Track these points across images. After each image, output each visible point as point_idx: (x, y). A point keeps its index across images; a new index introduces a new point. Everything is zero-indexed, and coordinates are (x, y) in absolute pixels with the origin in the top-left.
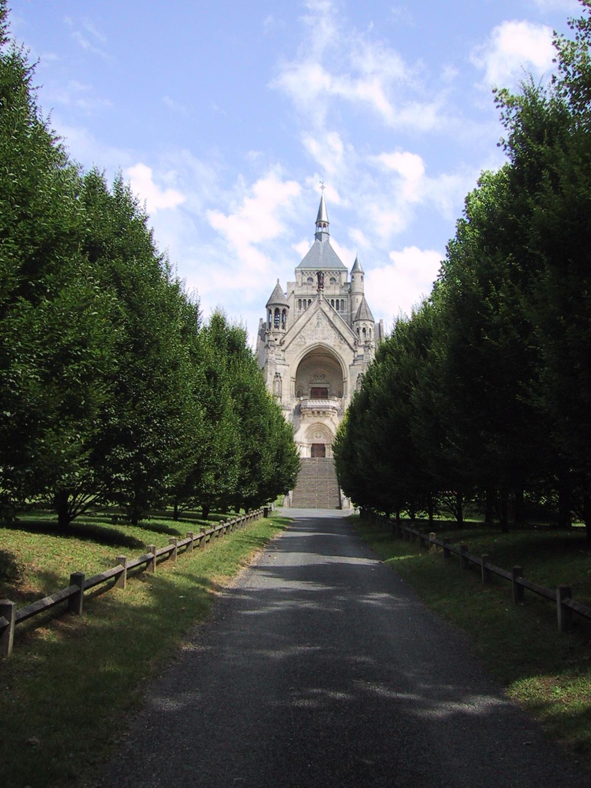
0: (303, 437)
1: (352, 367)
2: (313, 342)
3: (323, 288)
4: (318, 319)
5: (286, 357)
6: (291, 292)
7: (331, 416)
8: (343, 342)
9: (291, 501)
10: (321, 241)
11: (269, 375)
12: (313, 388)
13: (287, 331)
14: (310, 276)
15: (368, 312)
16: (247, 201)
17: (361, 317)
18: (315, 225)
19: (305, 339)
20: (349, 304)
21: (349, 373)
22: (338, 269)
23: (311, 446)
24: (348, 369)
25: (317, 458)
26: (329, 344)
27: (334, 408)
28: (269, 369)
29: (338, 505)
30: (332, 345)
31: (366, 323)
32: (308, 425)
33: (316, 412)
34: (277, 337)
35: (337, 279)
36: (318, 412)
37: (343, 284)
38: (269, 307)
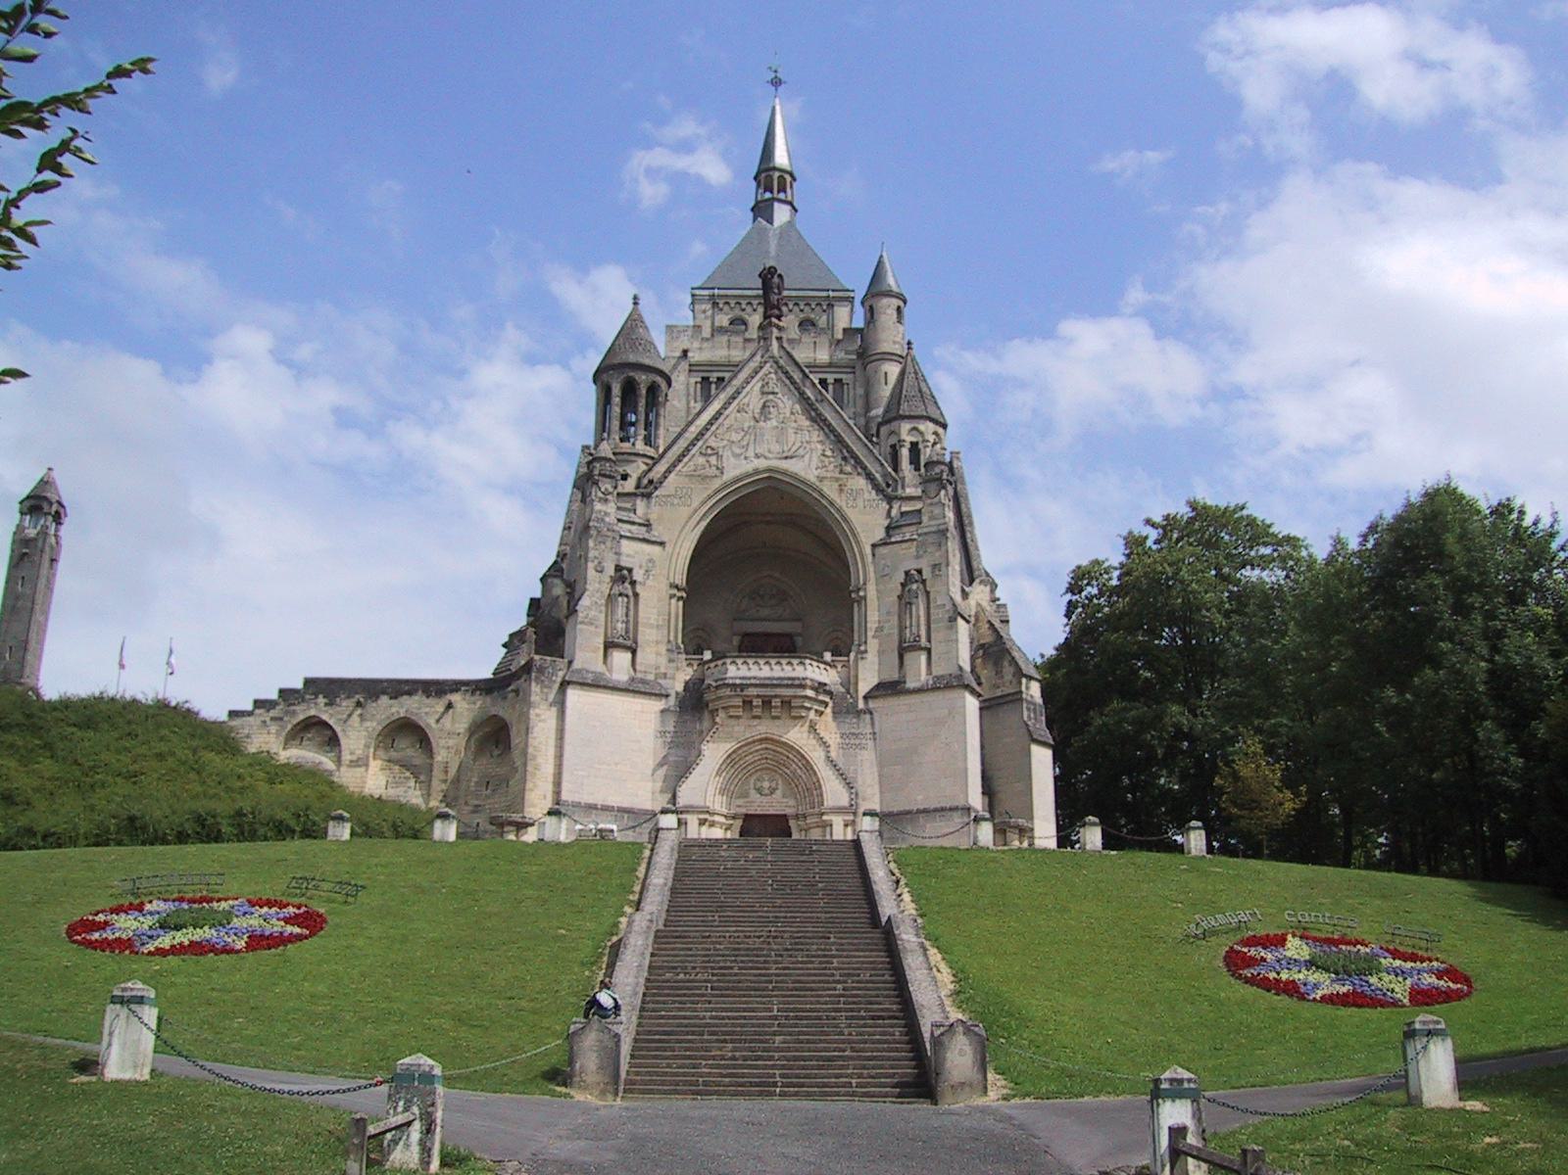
0: (711, 790)
2: (749, 467)
3: (779, 318)
4: (763, 393)
5: (653, 517)
6: (678, 354)
7: (812, 715)
8: (848, 469)
9: (626, 1048)
10: (771, 223)
11: (591, 573)
12: (746, 635)
13: (661, 450)
14: (737, 312)
15: (926, 397)
17: (904, 409)
19: (719, 457)
20: (860, 391)
21: (871, 569)
22: (825, 294)
23: (739, 823)
24: (870, 558)
25: (769, 841)
26: (802, 474)
27: (820, 687)
28: (591, 554)
29: (907, 1070)
30: (811, 476)
31: (922, 427)
32: (727, 747)
33: (757, 702)
34: (629, 469)
35: (822, 321)
36: (767, 703)
37: (839, 335)
38: (605, 377)
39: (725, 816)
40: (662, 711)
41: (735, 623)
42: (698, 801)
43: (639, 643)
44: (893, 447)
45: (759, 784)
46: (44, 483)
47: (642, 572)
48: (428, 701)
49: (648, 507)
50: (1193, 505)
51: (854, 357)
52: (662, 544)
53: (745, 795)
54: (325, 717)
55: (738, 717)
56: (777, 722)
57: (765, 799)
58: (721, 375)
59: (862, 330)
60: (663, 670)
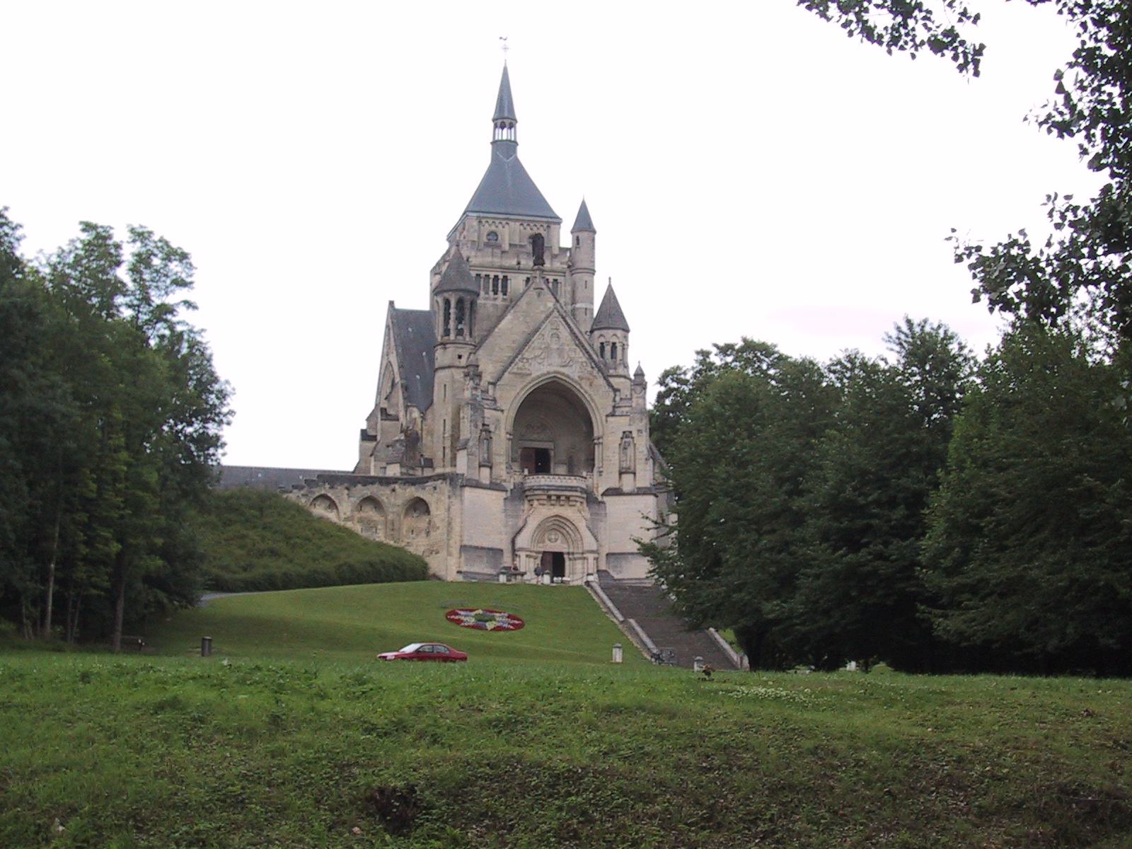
1: (610, 419)
5: (498, 395)
18: (492, 124)
20: (569, 288)
26: (571, 375)
40: (505, 499)
42: (525, 546)
47: (493, 426)
48: (383, 488)
49: (494, 390)
50: (745, 340)
52: (502, 411)
54: (329, 495)
55: (544, 505)
56: (562, 508)
57: (552, 544)
58: (488, 273)
59: (570, 249)
60: (504, 478)
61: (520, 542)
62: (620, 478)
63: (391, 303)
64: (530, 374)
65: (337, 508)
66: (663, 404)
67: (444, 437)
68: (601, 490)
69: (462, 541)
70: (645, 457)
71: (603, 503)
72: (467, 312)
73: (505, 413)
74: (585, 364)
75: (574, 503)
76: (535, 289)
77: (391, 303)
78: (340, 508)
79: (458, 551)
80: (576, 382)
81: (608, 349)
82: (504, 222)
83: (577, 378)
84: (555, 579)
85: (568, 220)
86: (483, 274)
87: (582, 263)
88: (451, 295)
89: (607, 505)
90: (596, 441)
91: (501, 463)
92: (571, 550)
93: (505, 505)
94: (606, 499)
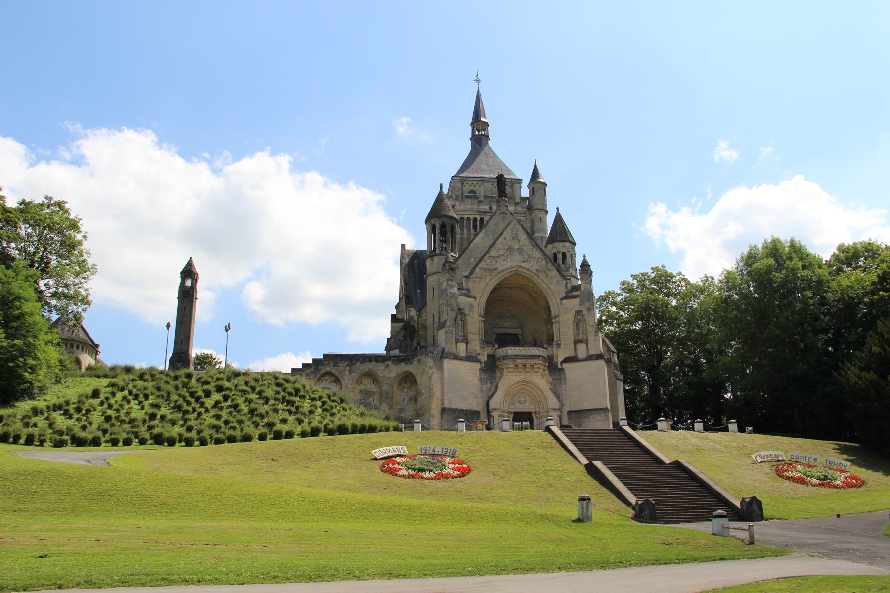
1: (564, 302)
5: (470, 286)
12: (499, 334)
16: (279, 156)
23: (512, 415)
26: (530, 268)
33: (520, 366)
39: (508, 413)
41: (494, 329)
42: (498, 407)
43: (469, 340)
44: (555, 254)
45: (519, 400)
46: (190, 264)
51: (525, 210)
52: (475, 298)
53: (514, 404)
56: (528, 374)
57: (521, 405)
60: (478, 352)
61: (494, 404)
62: (575, 346)
63: (403, 246)
64: (497, 269)
65: (340, 383)
66: (602, 318)
67: (433, 327)
68: (560, 359)
69: (442, 404)
70: (594, 330)
71: (562, 369)
72: (449, 234)
73: (478, 300)
74: (540, 260)
75: (538, 370)
76: (500, 214)
77: (403, 246)
78: (342, 382)
79: (440, 413)
80: (535, 274)
81: (560, 256)
82: (480, 183)
83: (534, 271)
84: (516, 423)
85: (526, 179)
86: (466, 217)
87: (536, 203)
88: (436, 221)
89: (566, 371)
90: (553, 320)
91: (475, 340)
92: (538, 410)
93: (480, 374)
94: (565, 366)
